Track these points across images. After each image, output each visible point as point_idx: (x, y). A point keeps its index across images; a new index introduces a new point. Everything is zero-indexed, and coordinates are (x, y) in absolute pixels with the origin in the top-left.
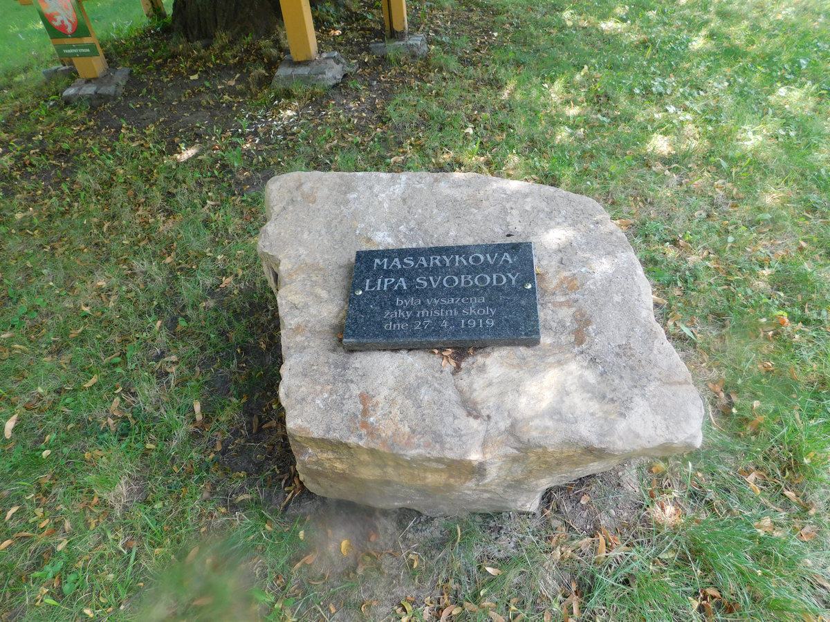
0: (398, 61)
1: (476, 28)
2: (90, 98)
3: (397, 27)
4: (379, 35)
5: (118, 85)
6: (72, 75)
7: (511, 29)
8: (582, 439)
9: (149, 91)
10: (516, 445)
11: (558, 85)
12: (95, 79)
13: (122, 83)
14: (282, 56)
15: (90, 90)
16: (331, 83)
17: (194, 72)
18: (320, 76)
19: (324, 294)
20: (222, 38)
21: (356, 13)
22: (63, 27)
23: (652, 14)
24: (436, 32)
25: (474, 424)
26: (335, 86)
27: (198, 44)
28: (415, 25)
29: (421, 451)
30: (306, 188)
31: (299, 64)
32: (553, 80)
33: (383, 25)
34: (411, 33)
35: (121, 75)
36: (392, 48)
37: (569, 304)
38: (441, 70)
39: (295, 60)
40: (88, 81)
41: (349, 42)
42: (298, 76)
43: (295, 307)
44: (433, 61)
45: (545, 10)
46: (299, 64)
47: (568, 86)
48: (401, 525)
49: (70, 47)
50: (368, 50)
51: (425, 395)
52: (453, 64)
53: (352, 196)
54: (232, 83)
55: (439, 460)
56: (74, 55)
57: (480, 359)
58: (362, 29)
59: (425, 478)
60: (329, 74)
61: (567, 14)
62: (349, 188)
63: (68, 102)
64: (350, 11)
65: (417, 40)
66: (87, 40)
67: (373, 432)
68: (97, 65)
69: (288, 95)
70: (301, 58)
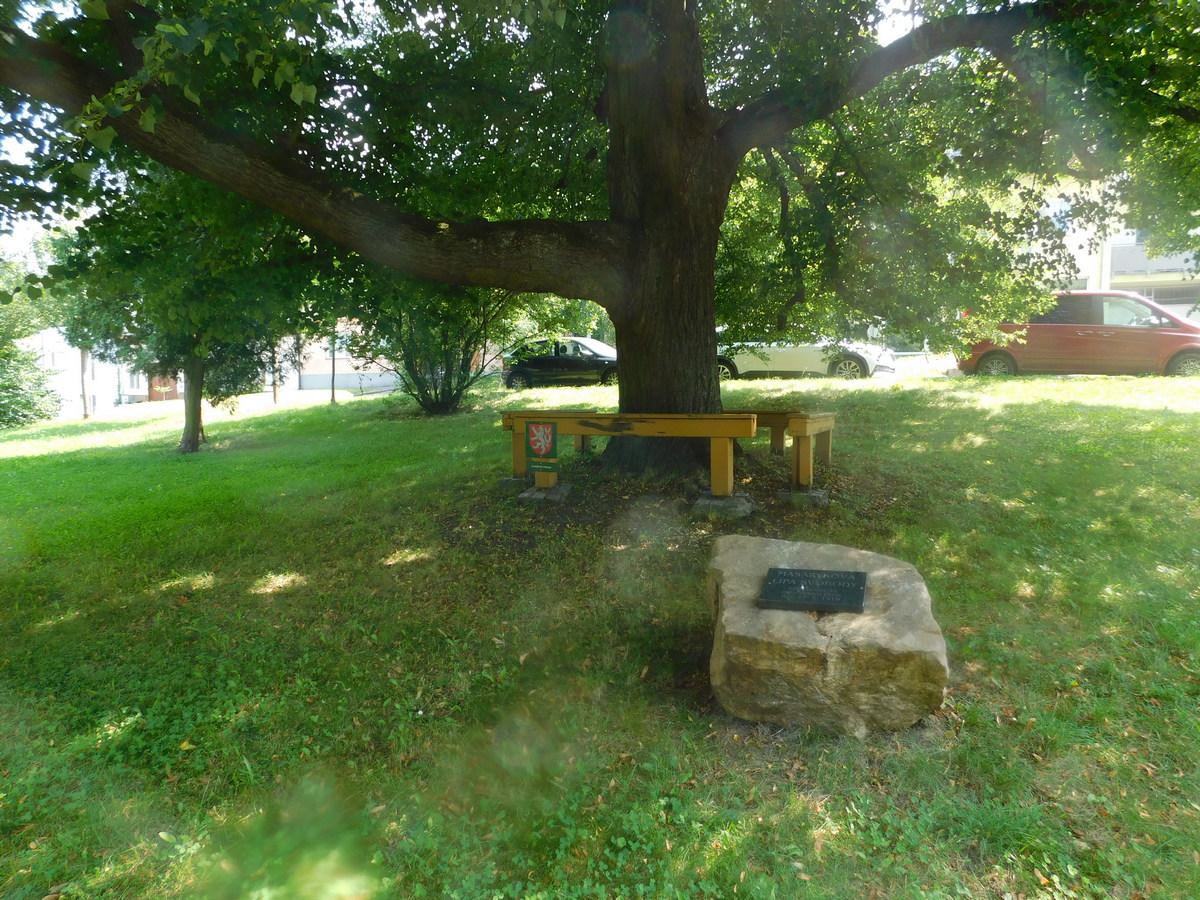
0: (800, 509)
1: (878, 492)
2: (539, 502)
3: (803, 481)
4: (787, 487)
5: (562, 494)
6: (531, 484)
7: (912, 497)
8: (877, 643)
9: (587, 503)
10: (845, 647)
11: (943, 541)
12: (546, 489)
13: (566, 494)
14: (705, 490)
15: (541, 496)
16: (741, 515)
17: (627, 494)
18: (733, 509)
19: (748, 586)
20: (650, 473)
21: (766, 468)
22: (540, 449)
23: (1061, 500)
24: (838, 491)
25: (823, 638)
26: (744, 518)
27: (629, 475)
28: (819, 482)
29: (795, 644)
30: (740, 543)
31: (717, 498)
32: (938, 535)
33: (790, 480)
34: (815, 489)
35: (565, 490)
36: (797, 498)
37: (883, 599)
38: (838, 518)
39: (714, 494)
40: (540, 490)
41: (759, 488)
42: (715, 507)
43: (732, 590)
44: (832, 511)
45: (949, 486)
46: (717, 498)
47: (951, 542)
48: (773, 731)
49: (536, 464)
50: (775, 497)
51: (799, 626)
52: (851, 516)
53: (767, 548)
54: (657, 505)
55: (802, 650)
56: (538, 470)
57: (831, 617)
58: (771, 480)
59: (794, 668)
60: (740, 508)
61: (970, 491)
62: (767, 545)
63: (520, 503)
64: (761, 466)
65: (820, 494)
66: (552, 461)
67: (770, 636)
68: (552, 478)
69: (705, 519)
70: (719, 493)
